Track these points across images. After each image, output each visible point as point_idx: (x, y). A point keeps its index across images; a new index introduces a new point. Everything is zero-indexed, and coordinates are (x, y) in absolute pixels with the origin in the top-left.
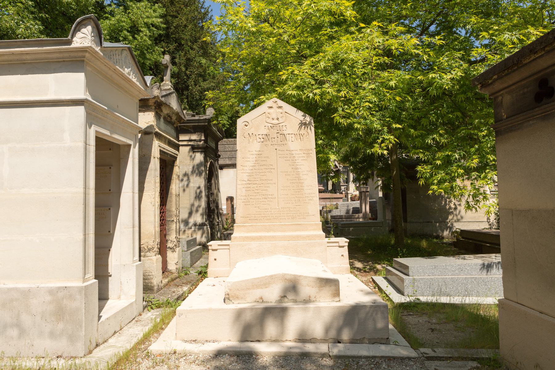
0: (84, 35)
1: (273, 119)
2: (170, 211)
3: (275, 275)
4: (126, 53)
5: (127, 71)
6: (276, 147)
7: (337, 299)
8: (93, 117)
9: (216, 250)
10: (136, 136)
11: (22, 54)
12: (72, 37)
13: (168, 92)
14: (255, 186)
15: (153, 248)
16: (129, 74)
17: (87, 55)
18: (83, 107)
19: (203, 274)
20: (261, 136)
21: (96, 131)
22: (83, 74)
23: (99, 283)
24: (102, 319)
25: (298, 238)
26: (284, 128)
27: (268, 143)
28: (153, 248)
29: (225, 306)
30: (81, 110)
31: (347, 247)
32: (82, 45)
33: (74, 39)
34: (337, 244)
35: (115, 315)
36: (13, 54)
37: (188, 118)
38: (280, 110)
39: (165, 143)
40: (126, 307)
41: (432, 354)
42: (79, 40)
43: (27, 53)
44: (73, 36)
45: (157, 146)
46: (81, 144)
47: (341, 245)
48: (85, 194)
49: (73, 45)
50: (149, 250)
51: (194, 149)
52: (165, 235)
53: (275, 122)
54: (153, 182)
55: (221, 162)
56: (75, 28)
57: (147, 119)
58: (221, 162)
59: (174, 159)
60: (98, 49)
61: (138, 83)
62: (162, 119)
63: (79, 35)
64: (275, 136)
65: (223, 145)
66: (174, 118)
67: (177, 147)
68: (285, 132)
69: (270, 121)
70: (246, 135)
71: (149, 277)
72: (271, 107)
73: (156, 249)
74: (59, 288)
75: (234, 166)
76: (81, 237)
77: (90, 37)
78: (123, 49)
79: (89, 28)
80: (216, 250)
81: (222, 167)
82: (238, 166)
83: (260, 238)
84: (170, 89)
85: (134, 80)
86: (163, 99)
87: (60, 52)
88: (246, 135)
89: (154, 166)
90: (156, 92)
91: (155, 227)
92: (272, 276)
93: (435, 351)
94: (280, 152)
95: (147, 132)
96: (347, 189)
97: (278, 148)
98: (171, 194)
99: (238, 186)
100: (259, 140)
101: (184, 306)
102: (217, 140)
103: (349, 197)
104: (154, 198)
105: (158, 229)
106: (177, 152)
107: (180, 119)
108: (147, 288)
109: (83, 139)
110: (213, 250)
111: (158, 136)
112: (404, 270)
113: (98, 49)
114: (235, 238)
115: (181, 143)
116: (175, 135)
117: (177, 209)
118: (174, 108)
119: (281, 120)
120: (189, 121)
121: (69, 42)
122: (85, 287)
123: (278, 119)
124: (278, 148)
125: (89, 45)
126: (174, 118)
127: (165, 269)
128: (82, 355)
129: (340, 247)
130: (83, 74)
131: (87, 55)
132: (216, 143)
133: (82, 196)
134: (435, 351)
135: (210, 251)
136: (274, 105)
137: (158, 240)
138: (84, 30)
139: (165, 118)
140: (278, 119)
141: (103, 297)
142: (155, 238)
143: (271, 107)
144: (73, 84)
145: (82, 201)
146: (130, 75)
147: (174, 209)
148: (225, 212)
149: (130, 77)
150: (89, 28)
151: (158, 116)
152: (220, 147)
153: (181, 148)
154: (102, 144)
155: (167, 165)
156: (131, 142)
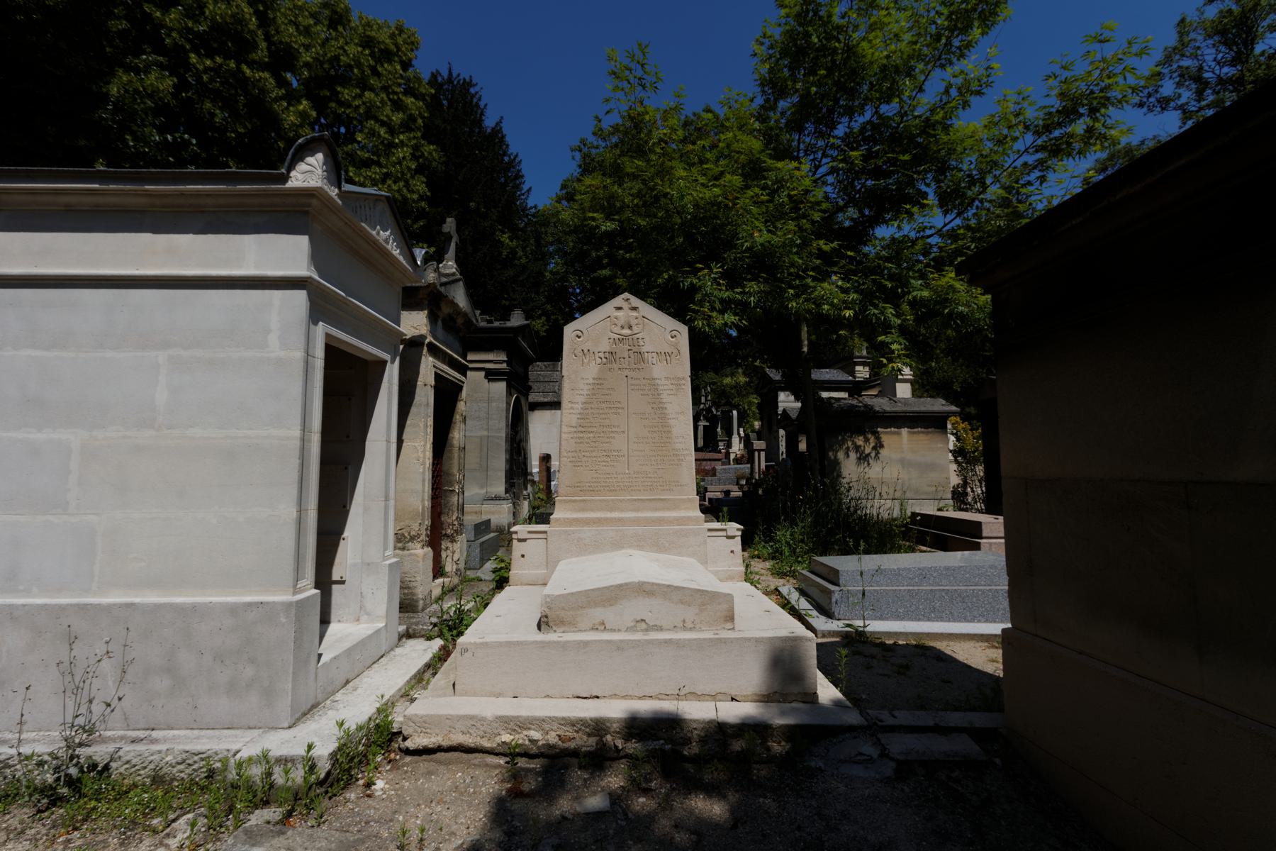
0: (309, 168)
1: (622, 327)
2: (449, 474)
3: (626, 584)
4: (383, 206)
5: (385, 234)
6: (627, 372)
7: (729, 625)
8: (321, 308)
9: (524, 540)
10: (396, 348)
11: (198, 194)
12: (289, 171)
13: (452, 278)
15: (419, 536)
16: (387, 241)
17: (314, 202)
18: (304, 292)
19: (501, 582)
20: (602, 355)
21: (328, 335)
22: (306, 238)
23: (322, 594)
24: (323, 660)
25: (660, 521)
27: (615, 366)
28: (419, 536)
29: (540, 637)
30: (301, 296)
31: (739, 539)
32: (306, 185)
33: (293, 174)
35: (349, 652)
36: (182, 194)
37: (483, 324)
38: (635, 314)
39: (444, 362)
40: (370, 637)
41: (890, 721)
42: (299, 176)
43: (209, 195)
44: (290, 169)
45: (428, 367)
46: (299, 354)
47: (730, 533)
48: (303, 440)
49: (290, 184)
50: (412, 539)
51: (491, 375)
52: (440, 514)
54: (422, 425)
55: (533, 397)
56: (294, 155)
57: (414, 323)
58: (533, 397)
59: (458, 388)
60: (333, 192)
61: (401, 258)
62: (440, 323)
63: (302, 167)
64: (626, 355)
65: (538, 371)
66: (460, 321)
67: (463, 370)
68: (644, 349)
69: (616, 329)
70: (578, 351)
71: (411, 585)
72: (620, 308)
73: (423, 537)
74: (250, 605)
75: (556, 405)
76: (294, 513)
77: (320, 172)
78: (377, 198)
79: (320, 156)
80: (524, 540)
81: (535, 406)
82: (565, 404)
83: (598, 521)
84: (453, 274)
85: (396, 252)
86: (442, 289)
87: (265, 194)
88: (578, 351)
89: (425, 396)
90: (431, 277)
91: (423, 500)
92: (621, 585)
93: (894, 717)
94: (634, 382)
95: (415, 344)
96: (729, 445)
97: (630, 374)
98: (452, 446)
99: (564, 436)
100: (599, 361)
101: (470, 636)
102: (528, 362)
103: (732, 456)
104: (424, 451)
105: (428, 504)
106: (463, 378)
107: (468, 323)
108: (407, 606)
109: (302, 345)
110: (520, 540)
111: (433, 350)
112: (833, 576)
113: (333, 192)
114: (557, 520)
115: (471, 366)
116: (461, 350)
117: (460, 470)
118: (461, 305)
119: (636, 329)
120: (483, 329)
121: (285, 178)
122: (297, 602)
123: (630, 327)
124: (630, 374)
125: (319, 184)
126: (460, 321)
127: (438, 571)
128: (286, 725)
129: (729, 537)
130: (306, 238)
131: (314, 202)
132: (529, 365)
133: (298, 443)
134: (894, 717)
135: (515, 542)
136: (625, 305)
137: (428, 522)
138: (310, 160)
139: (444, 321)
141: (325, 621)
142: (423, 519)
143: (620, 308)
144: (288, 254)
145: (297, 453)
146: (387, 243)
147: (455, 471)
148: (536, 478)
149: (389, 247)
150: (320, 156)
151: (433, 318)
152: (532, 374)
153: (469, 373)
154: (335, 356)
155: (447, 396)
156: (387, 357)
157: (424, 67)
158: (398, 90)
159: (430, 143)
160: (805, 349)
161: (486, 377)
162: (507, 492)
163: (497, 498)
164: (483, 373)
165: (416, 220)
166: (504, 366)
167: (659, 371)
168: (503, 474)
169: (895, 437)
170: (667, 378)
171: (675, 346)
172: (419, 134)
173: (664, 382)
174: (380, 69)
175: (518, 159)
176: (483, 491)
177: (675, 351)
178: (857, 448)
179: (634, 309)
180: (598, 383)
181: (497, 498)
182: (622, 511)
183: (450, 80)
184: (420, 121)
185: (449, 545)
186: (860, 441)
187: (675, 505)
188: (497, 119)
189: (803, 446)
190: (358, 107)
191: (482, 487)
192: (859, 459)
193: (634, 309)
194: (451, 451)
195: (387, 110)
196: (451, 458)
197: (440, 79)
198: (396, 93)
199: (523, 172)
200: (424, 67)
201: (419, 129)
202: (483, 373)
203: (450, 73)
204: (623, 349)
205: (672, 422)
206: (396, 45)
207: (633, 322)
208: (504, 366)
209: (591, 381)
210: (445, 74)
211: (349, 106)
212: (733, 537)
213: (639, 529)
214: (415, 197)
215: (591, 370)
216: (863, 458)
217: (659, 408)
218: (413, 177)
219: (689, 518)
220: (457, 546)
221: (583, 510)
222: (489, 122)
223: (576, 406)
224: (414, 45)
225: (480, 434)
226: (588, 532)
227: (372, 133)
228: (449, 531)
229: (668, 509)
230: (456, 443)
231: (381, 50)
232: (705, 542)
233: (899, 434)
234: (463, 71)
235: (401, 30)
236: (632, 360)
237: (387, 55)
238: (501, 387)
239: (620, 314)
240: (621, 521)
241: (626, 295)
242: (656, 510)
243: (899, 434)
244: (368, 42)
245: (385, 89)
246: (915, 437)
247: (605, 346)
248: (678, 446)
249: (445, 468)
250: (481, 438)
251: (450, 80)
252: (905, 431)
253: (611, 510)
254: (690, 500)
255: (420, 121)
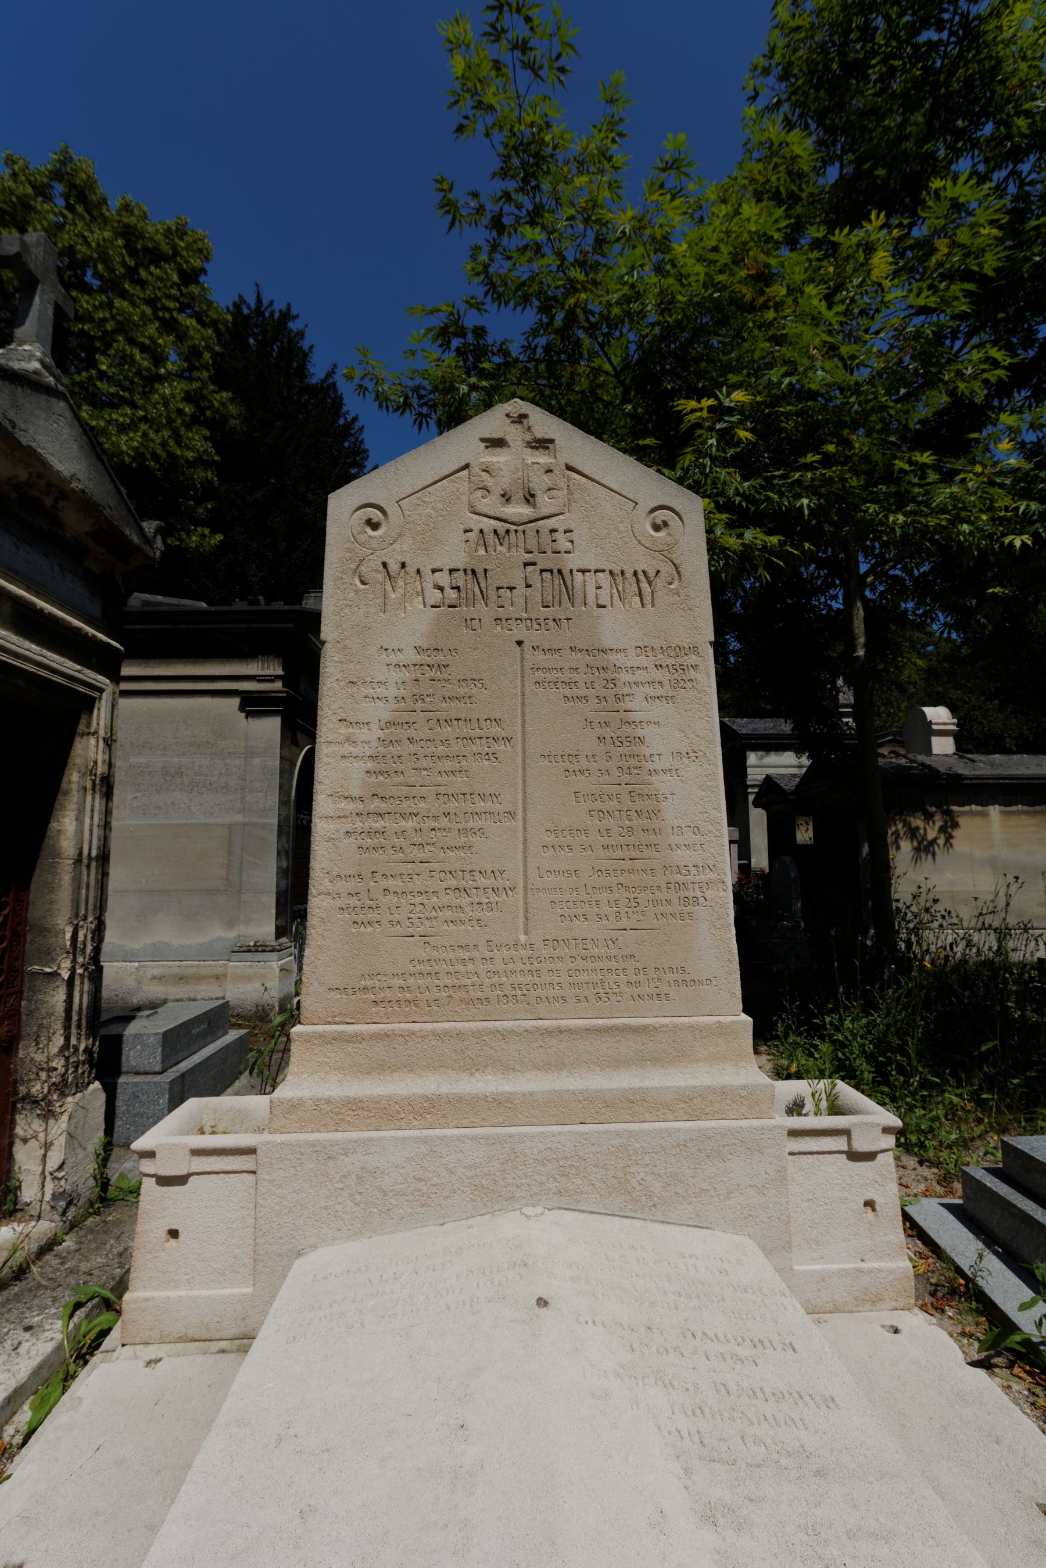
2: (45, 930)
6: (520, 631)
9: (181, 1180)
14: (410, 824)
20: (443, 579)
26: (563, 543)
34: (841, 1144)
38: (543, 458)
47: (860, 1145)
53: (518, 510)
64: (519, 576)
68: (572, 562)
69: (490, 504)
72: (496, 443)
80: (181, 1180)
83: (429, 1110)
94: (542, 659)
97: (532, 637)
98: (56, 853)
107: (108, 535)
110: (164, 1181)
119: (546, 504)
123: (530, 498)
124: (532, 637)
129: (854, 1156)
136: (515, 435)
140: (530, 498)
157: (224, 288)
158: (171, 304)
159: (222, 388)
160: (861, 653)
161: (242, 708)
162: (280, 932)
163: (259, 948)
164: (236, 701)
165: (200, 501)
166: (278, 685)
167: (619, 627)
168: (270, 900)
169: (978, 821)
170: (642, 649)
171: (666, 553)
172: (205, 374)
173: (634, 659)
174: (143, 273)
175: (357, 425)
176: (231, 934)
177: (666, 569)
178: (913, 833)
179: (542, 444)
180: (433, 663)
181: (259, 948)
182: (507, 1068)
183: (259, 311)
184: (207, 356)
185: (37, 1125)
186: (917, 822)
187: (674, 1048)
188: (328, 367)
189: (804, 835)
190: (103, 321)
191: (230, 924)
192: (917, 850)
193: (542, 444)
194: (54, 866)
195: (152, 329)
196: (51, 888)
197: (246, 311)
198: (169, 310)
199: (367, 445)
200: (224, 288)
201: (206, 367)
202: (236, 701)
203: (259, 300)
204: (507, 563)
205: (662, 783)
206: (174, 247)
207: (539, 482)
208: (278, 685)
209: (410, 656)
210: (252, 300)
211: (91, 320)
212: (869, 1156)
213: (560, 1132)
214: (190, 455)
215: (412, 624)
216: (925, 848)
217: (623, 741)
218: (188, 427)
219: (724, 1093)
220: (59, 1127)
221: (380, 1068)
222: (317, 371)
223: (361, 733)
224: (205, 255)
225: (227, 819)
226: (394, 1146)
227: (125, 359)
228: (37, 1089)
229: (657, 1061)
230: (67, 845)
231: (145, 249)
232: (782, 1175)
233: (985, 815)
234: (277, 298)
235: (181, 232)
236: (535, 594)
237: (156, 257)
238: (270, 727)
239: (499, 458)
240: (504, 1108)
241: (516, 406)
242: (617, 1063)
243: (985, 815)
244: (129, 234)
245: (150, 302)
246: (1014, 820)
247: (454, 552)
248: (682, 857)
249: (34, 914)
250: (230, 827)
251: (259, 311)
252: (994, 810)
253: (473, 1066)
254: (723, 1030)
255: (207, 356)
